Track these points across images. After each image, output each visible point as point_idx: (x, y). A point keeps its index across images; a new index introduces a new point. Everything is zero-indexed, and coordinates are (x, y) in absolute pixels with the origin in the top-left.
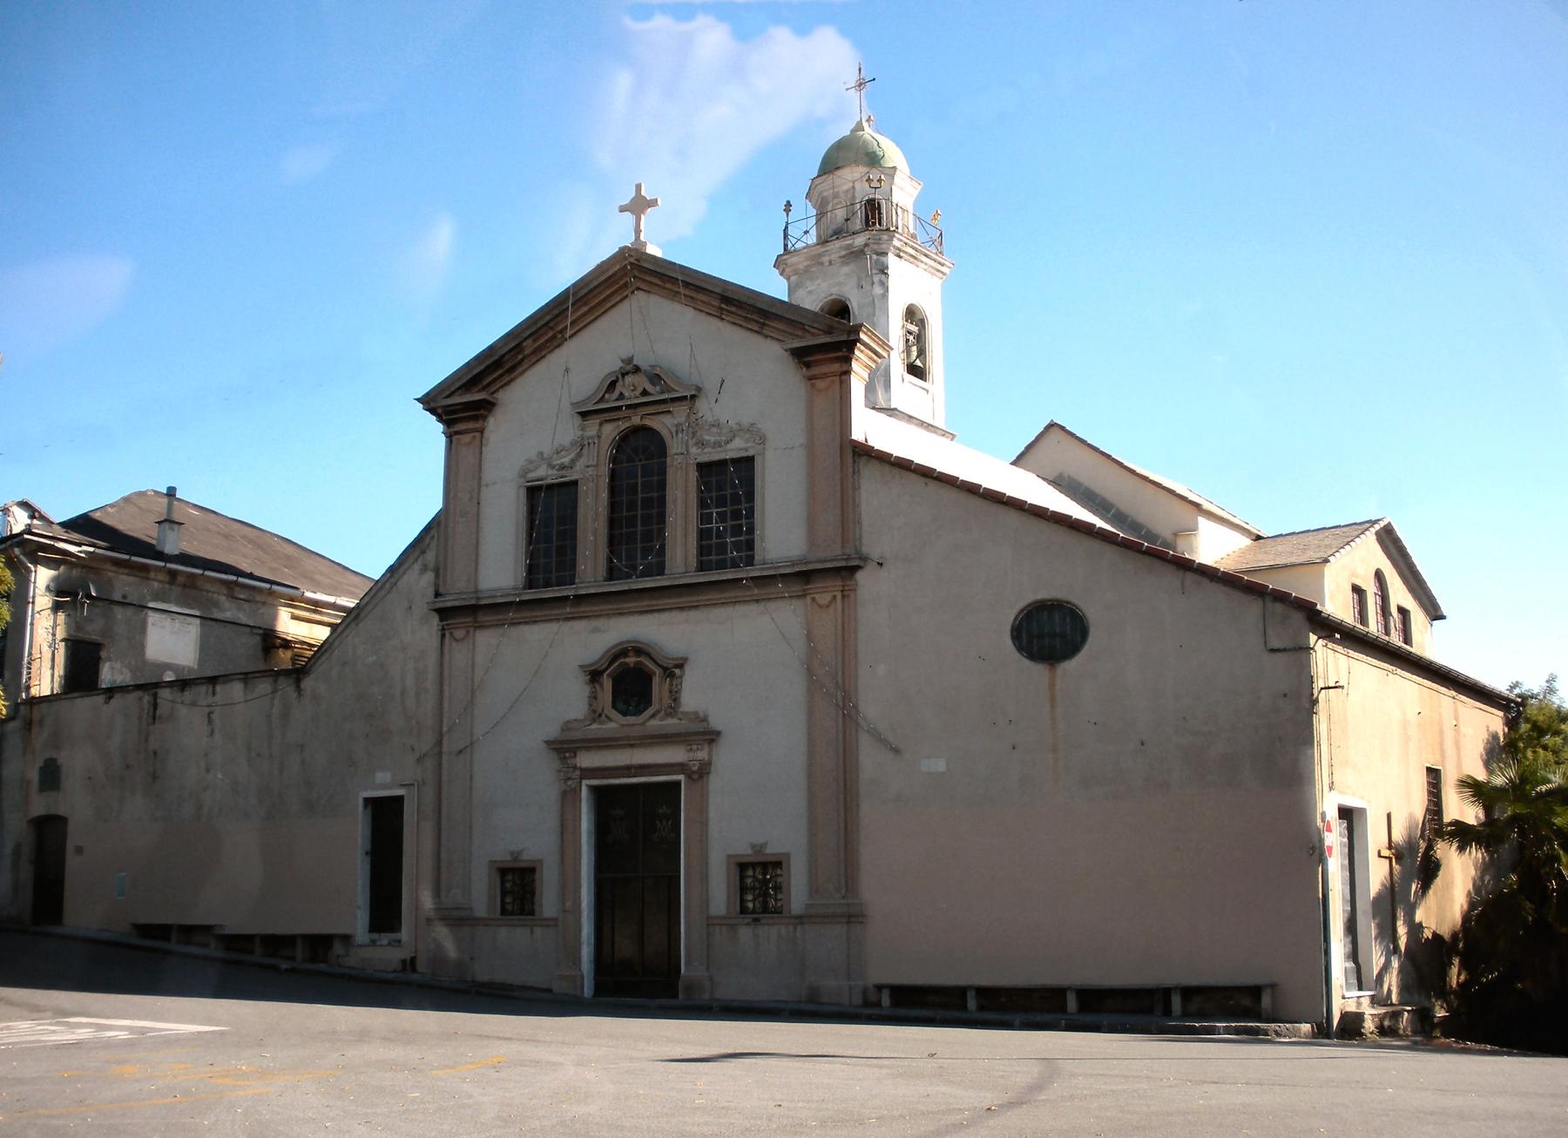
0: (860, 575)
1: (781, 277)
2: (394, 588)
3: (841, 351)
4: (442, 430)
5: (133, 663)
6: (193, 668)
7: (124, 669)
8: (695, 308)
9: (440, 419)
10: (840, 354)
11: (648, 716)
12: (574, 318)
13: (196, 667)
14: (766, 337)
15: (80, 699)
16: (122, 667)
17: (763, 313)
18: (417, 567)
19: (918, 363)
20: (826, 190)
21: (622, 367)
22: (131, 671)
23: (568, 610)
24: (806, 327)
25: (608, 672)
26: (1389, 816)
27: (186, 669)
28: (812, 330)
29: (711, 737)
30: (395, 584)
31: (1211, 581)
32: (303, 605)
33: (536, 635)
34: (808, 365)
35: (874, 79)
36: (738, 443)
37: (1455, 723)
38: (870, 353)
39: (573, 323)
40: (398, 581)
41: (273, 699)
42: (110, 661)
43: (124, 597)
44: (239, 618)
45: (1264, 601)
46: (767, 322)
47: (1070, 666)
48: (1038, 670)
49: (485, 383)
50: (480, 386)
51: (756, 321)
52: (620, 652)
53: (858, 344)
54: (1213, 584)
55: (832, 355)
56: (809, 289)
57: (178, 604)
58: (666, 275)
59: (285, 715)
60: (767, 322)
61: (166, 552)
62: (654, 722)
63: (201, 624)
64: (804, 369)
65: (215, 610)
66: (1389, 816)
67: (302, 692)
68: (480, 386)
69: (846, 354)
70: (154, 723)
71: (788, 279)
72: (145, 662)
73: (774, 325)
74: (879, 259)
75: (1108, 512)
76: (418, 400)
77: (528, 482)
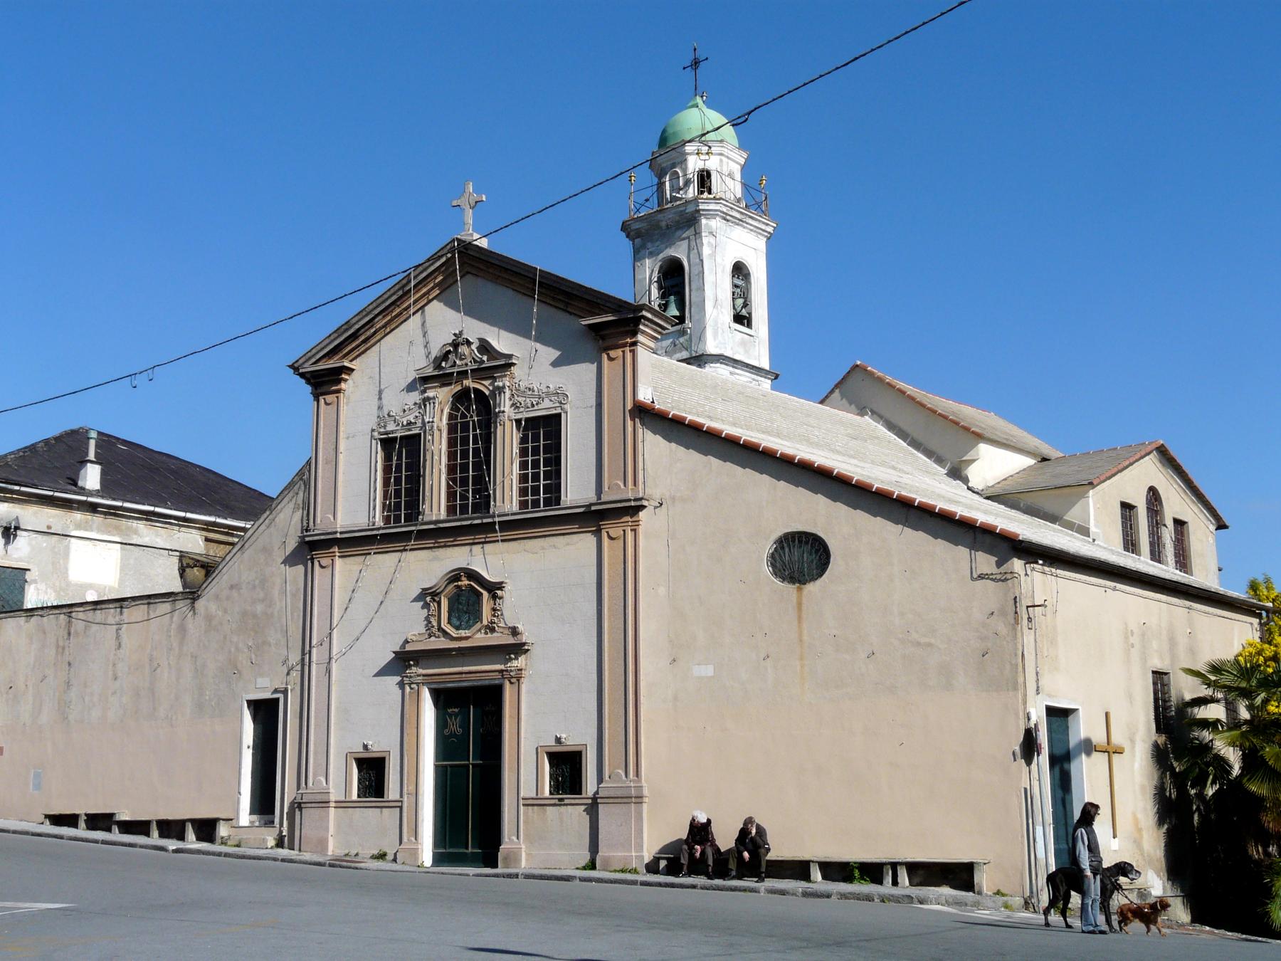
0: (642, 514)
1: (628, 239)
2: (273, 524)
3: (629, 326)
4: (310, 391)
5: (57, 584)
6: (114, 588)
7: (49, 590)
8: (514, 290)
9: (308, 382)
10: (628, 328)
11: (475, 631)
12: (415, 298)
13: (116, 586)
14: (571, 313)
15: (627, 219)
16: (47, 589)
17: (569, 295)
18: (291, 505)
19: (744, 312)
20: (663, 163)
21: (454, 340)
22: (55, 591)
23: (412, 543)
24: (602, 307)
25: (444, 593)
26: (1107, 715)
27: (107, 589)
28: (606, 308)
29: (518, 649)
30: (274, 520)
31: (931, 517)
32: (222, 530)
33: (383, 563)
34: (603, 338)
35: (707, 59)
36: (546, 403)
37: (1189, 631)
38: (654, 327)
39: (415, 302)
40: (276, 517)
41: (172, 617)
42: (36, 583)
43: (49, 527)
44: (157, 542)
45: (975, 534)
46: (570, 302)
47: (812, 588)
48: (790, 589)
49: (344, 352)
50: (341, 355)
51: (563, 301)
52: (455, 576)
53: (642, 320)
54: (932, 518)
55: (622, 329)
56: (650, 250)
57: (99, 530)
58: (489, 262)
59: (182, 629)
60: (570, 302)
61: (87, 487)
62: (479, 635)
63: (121, 548)
64: (601, 341)
65: (135, 536)
66: (1107, 715)
67: (196, 611)
68: (341, 355)
69: (633, 328)
70: (69, 638)
71: (633, 240)
72: (68, 584)
73: (576, 304)
74: (707, 224)
75: (925, 448)
76: (289, 366)
77: (381, 435)
